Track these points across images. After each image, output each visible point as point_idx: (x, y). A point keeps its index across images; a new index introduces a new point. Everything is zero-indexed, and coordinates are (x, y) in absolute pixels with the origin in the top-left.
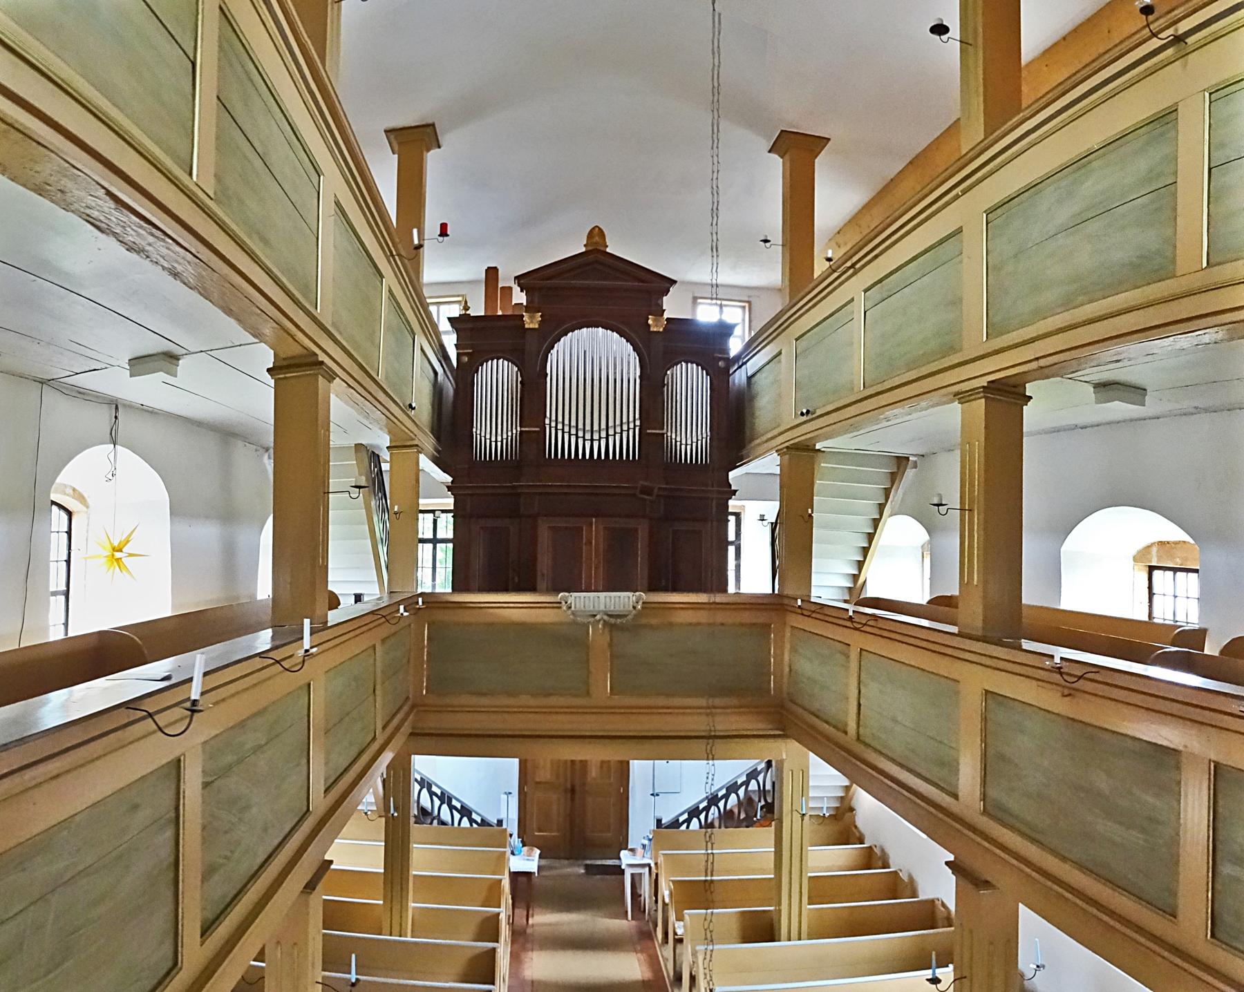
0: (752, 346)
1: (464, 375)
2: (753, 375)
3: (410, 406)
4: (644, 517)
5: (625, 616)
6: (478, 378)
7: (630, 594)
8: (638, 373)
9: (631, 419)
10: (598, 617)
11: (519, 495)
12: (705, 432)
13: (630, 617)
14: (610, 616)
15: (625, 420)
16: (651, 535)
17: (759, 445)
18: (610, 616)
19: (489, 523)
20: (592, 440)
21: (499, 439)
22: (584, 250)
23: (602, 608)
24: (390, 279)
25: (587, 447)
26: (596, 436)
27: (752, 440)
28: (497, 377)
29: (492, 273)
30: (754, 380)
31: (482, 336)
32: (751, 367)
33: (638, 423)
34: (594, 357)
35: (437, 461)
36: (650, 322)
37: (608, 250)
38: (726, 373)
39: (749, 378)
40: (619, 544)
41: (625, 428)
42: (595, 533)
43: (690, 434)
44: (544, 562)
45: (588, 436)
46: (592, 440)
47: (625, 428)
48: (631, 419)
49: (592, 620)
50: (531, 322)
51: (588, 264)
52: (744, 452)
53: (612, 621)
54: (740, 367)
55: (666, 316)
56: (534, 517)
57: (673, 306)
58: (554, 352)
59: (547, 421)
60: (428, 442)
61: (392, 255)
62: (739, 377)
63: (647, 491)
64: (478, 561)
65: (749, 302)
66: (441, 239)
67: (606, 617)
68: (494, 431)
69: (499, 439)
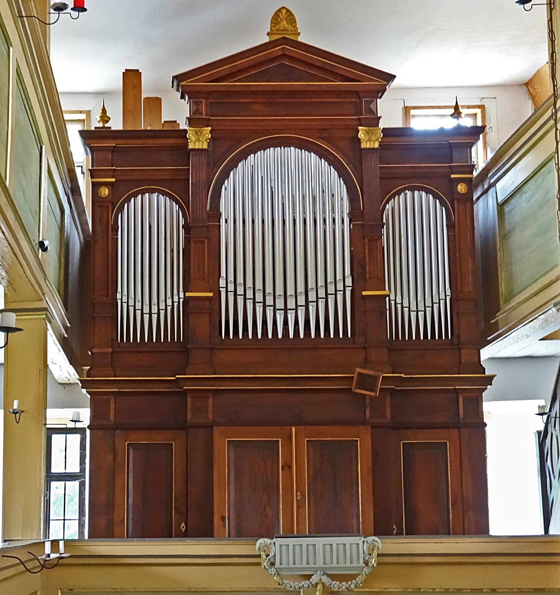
0: (501, 161)
1: (107, 210)
2: (506, 201)
3: (41, 244)
4: (364, 423)
5: (353, 577)
6: (123, 220)
7: (358, 540)
8: (346, 210)
9: (339, 276)
10: (314, 579)
11: (184, 394)
12: (443, 291)
13: (360, 579)
14: (333, 577)
15: (330, 279)
16: (375, 453)
17: (514, 308)
18: (333, 577)
19: (142, 438)
20: (286, 310)
21: (155, 309)
22: (267, 39)
23: (320, 564)
24: (16, 52)
25: (284, 317)
26: (291, 304)
27: (510, 296)
28: (151, 217)
29: (132, 78)
30: (507, 209)
31: (132, 156)
32: (506, 185)
33: (349, 282)
34: (283, 193)
35: (65, 344)
36: (361, 135)
37: (300, 39)
38: (468, 201)
39: (501, 207)
40: (331, 467)
41: (331, 290)
42: (295, 449)
43: (420, 294)
44: (224, 501)
45: (280, 304)
46: (286, 310)
47: (331, 290)
48: (339, 276)
49: (306, 583)
50: (199, 140)
51: (274, 59)
52: (500, 317)
53: (335, 585)
54: (486, 192)
55: (382, 124)
56: (209, 427)
57: (389, 112)
58: (228, 184)
59: (222, 283)
60: (57, 309)
61: (21, 17)
62: (485, 209)
63: (366, 382)
64: (127, 501)
65: (482, 107)
66: (75, 14)
67: (325, 579)
68: (147, 296)
69: (155, 309)
